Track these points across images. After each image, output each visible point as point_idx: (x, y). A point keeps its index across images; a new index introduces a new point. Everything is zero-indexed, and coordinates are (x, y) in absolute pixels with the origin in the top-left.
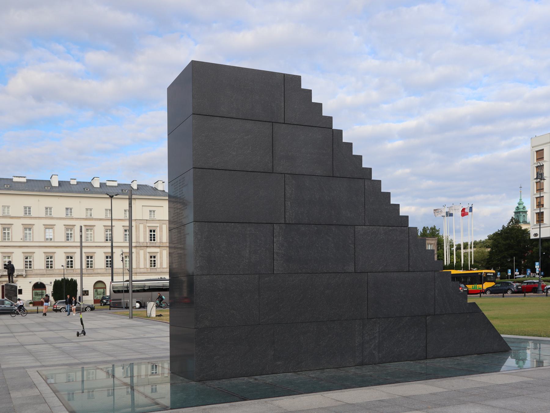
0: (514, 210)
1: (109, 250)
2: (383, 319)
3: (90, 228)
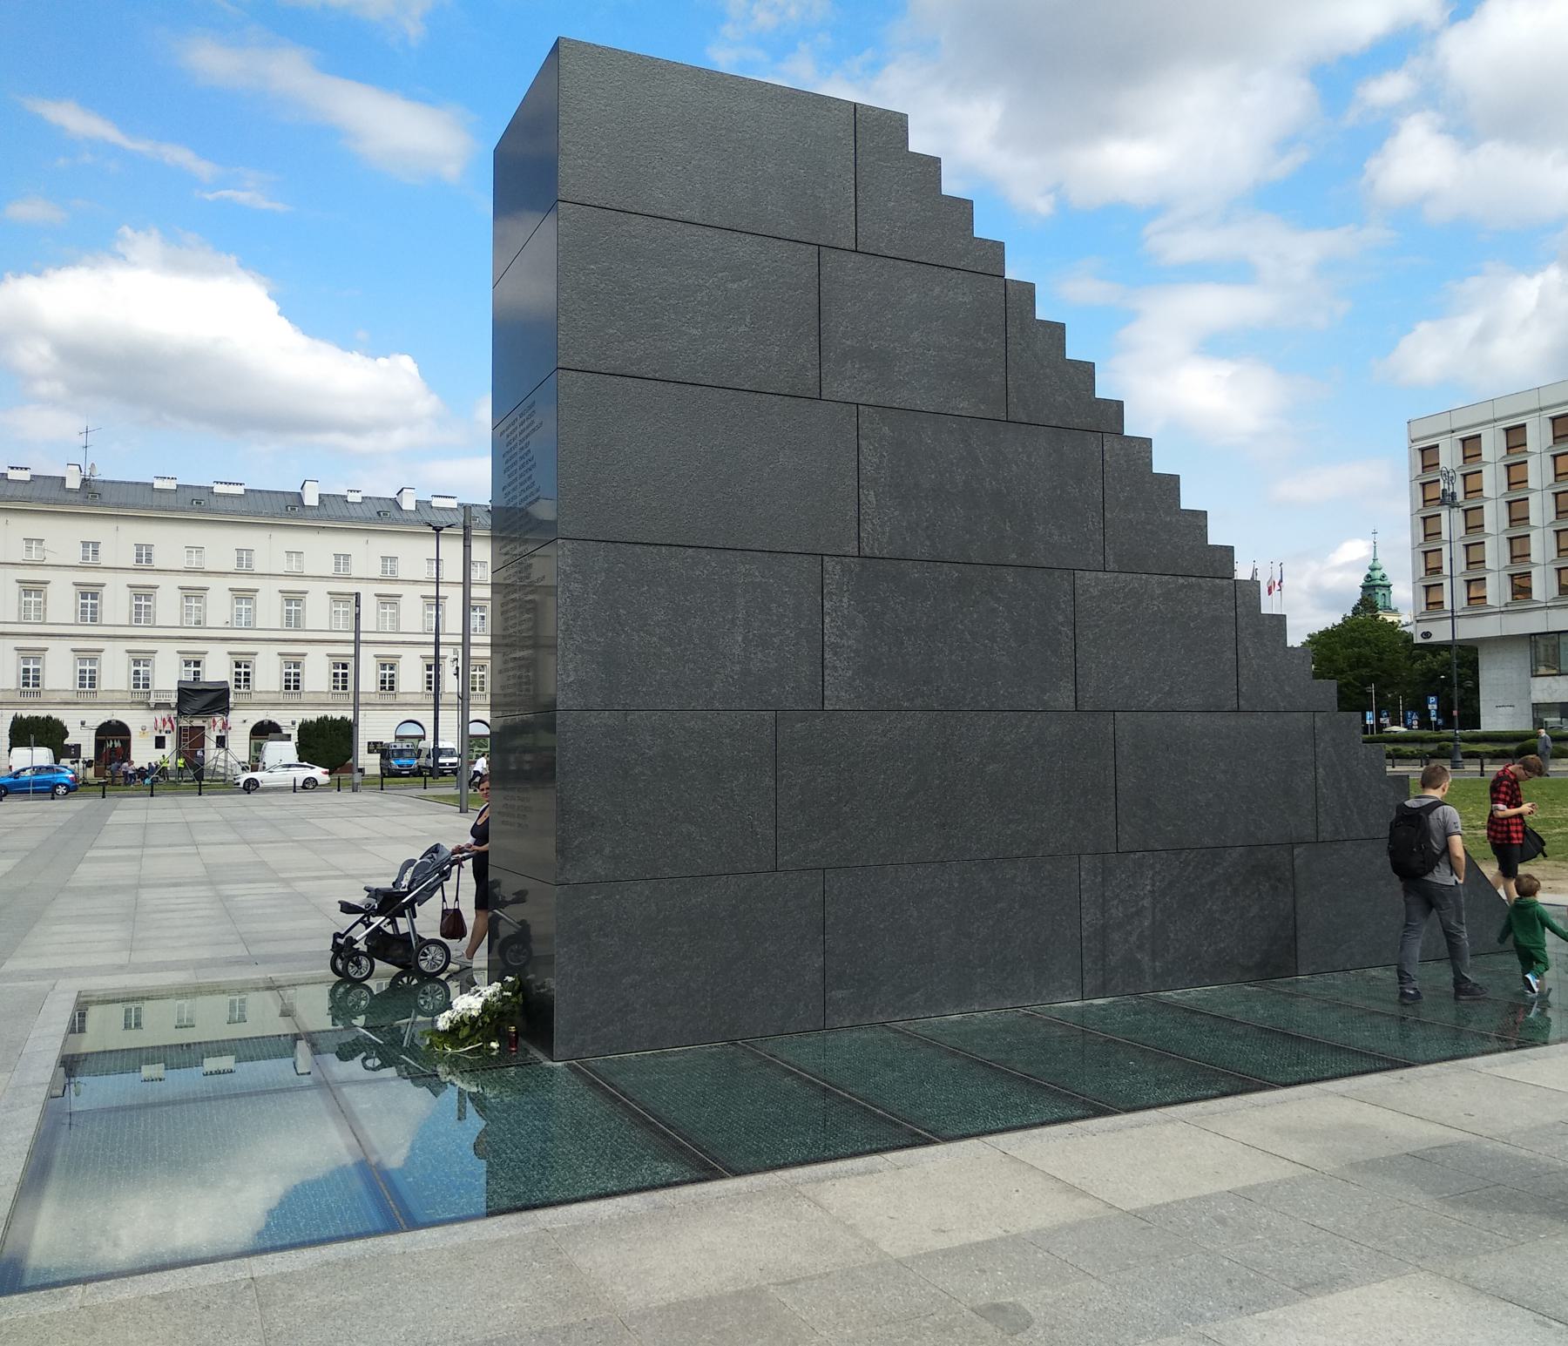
1: (431, 651)
2: (1164, 855)
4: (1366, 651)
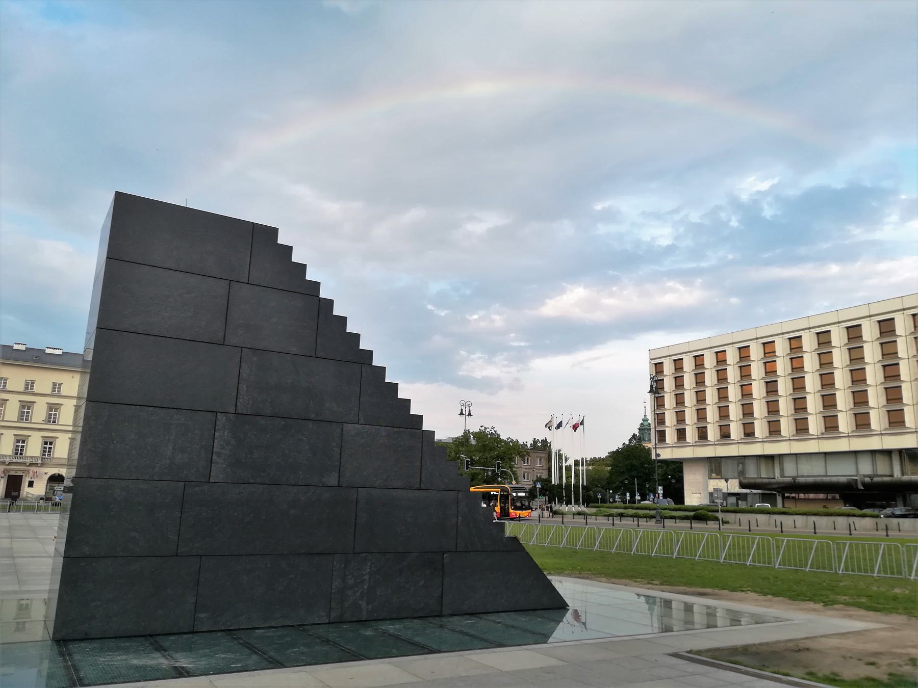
4: (634, 462)
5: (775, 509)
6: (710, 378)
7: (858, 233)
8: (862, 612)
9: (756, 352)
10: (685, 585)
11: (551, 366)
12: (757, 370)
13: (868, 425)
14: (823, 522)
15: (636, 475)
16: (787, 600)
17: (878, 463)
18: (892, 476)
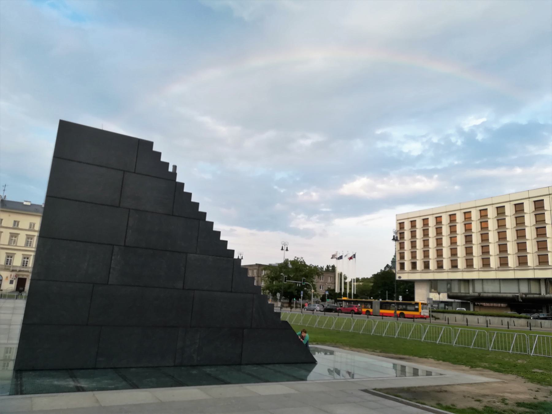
0: (391, 260)
3: (16, 235)
5: (468, 312)
6: (432, 232)
7: (533, 150)
8: (492, 372)
9: (460, 218)
10: (395, 353)
11: (346, 224)
12: (460, 229)
13: (526, 263)
14: (495, 321)
15: (387, 288)
16: (450, 364)
17: (532, 287)
18: (540, 294)
